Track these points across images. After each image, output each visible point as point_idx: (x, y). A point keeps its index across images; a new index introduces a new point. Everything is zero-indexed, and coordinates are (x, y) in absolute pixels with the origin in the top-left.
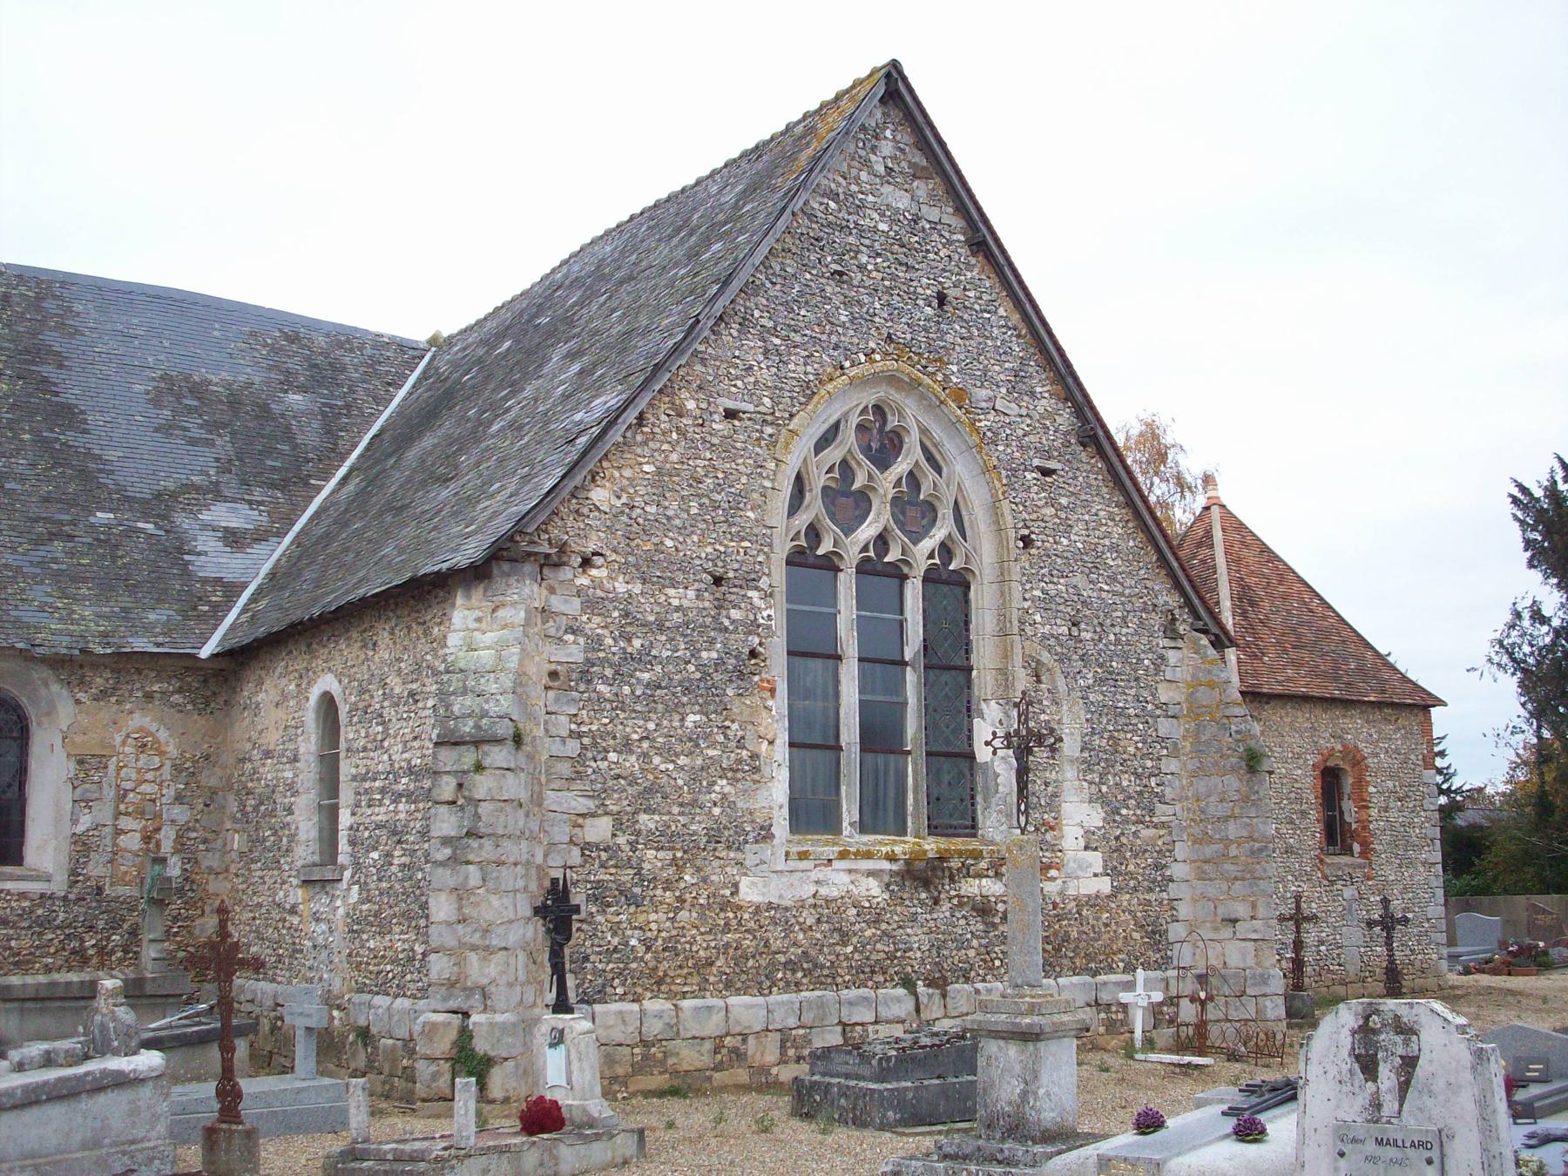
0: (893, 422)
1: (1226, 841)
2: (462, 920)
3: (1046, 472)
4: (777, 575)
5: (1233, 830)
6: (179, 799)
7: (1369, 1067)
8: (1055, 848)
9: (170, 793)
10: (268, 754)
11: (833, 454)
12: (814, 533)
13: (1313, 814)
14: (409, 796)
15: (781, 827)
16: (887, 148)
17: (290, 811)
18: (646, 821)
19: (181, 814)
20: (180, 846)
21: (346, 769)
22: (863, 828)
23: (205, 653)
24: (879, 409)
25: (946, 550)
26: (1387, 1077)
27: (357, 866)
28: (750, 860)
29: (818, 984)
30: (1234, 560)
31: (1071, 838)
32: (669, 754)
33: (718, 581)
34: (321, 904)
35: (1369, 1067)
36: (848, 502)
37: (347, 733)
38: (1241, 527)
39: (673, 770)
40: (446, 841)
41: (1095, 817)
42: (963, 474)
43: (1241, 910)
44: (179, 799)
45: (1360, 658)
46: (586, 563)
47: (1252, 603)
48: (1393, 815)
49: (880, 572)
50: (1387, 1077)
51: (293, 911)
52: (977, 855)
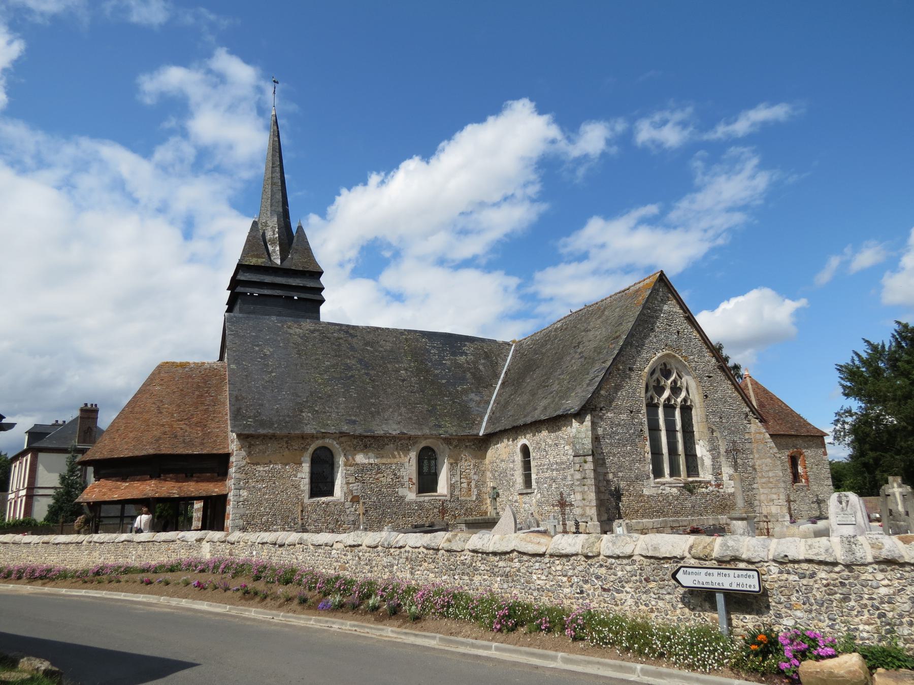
0: (668, 367)
1: (769, 477)
2: (584, 499)
3: (710, 377)
4: (644, 410)
5: (771, 474)
6: (475, 474)
7: (841, 503)
8: (721, 480)
9: (473, 472)
10: (502, 461)
11: (655, 376)
12: (652, 398)
13: (789, 470)
14: (557, 470)
15: (652, 476)
16: (661, 294)
17: (513, 475)
18: (620, 474)
19: (476, 477)
20: (476, 486)
21: (533, 464)
22: (331, 493)
23: (481, 434)
24: (665, 364)
25: (685, 400)
26: (844, 504)
27: (539, 488)
28: (645, 484)
29: (664, 516)
30: (756, 394)
31: (725, 477)
32: (623, 456)
33: (631, 412)
34: (526, 498)
35: (841, 503)
36: (660, 390)
37: (532, 455)
38: (757, 383)
39: (626, 461)
40: (578, 480)
41: (731, 471)
42: (688, 380)
43: (775, 497)
44: (475, 474)
45: (799, 422)
46: (601, 409)
47: (764, 407)
48: (814, 470)
49: (669, 408)
50: (844, 504)
51: (516, 501)
52: (700, 482)
